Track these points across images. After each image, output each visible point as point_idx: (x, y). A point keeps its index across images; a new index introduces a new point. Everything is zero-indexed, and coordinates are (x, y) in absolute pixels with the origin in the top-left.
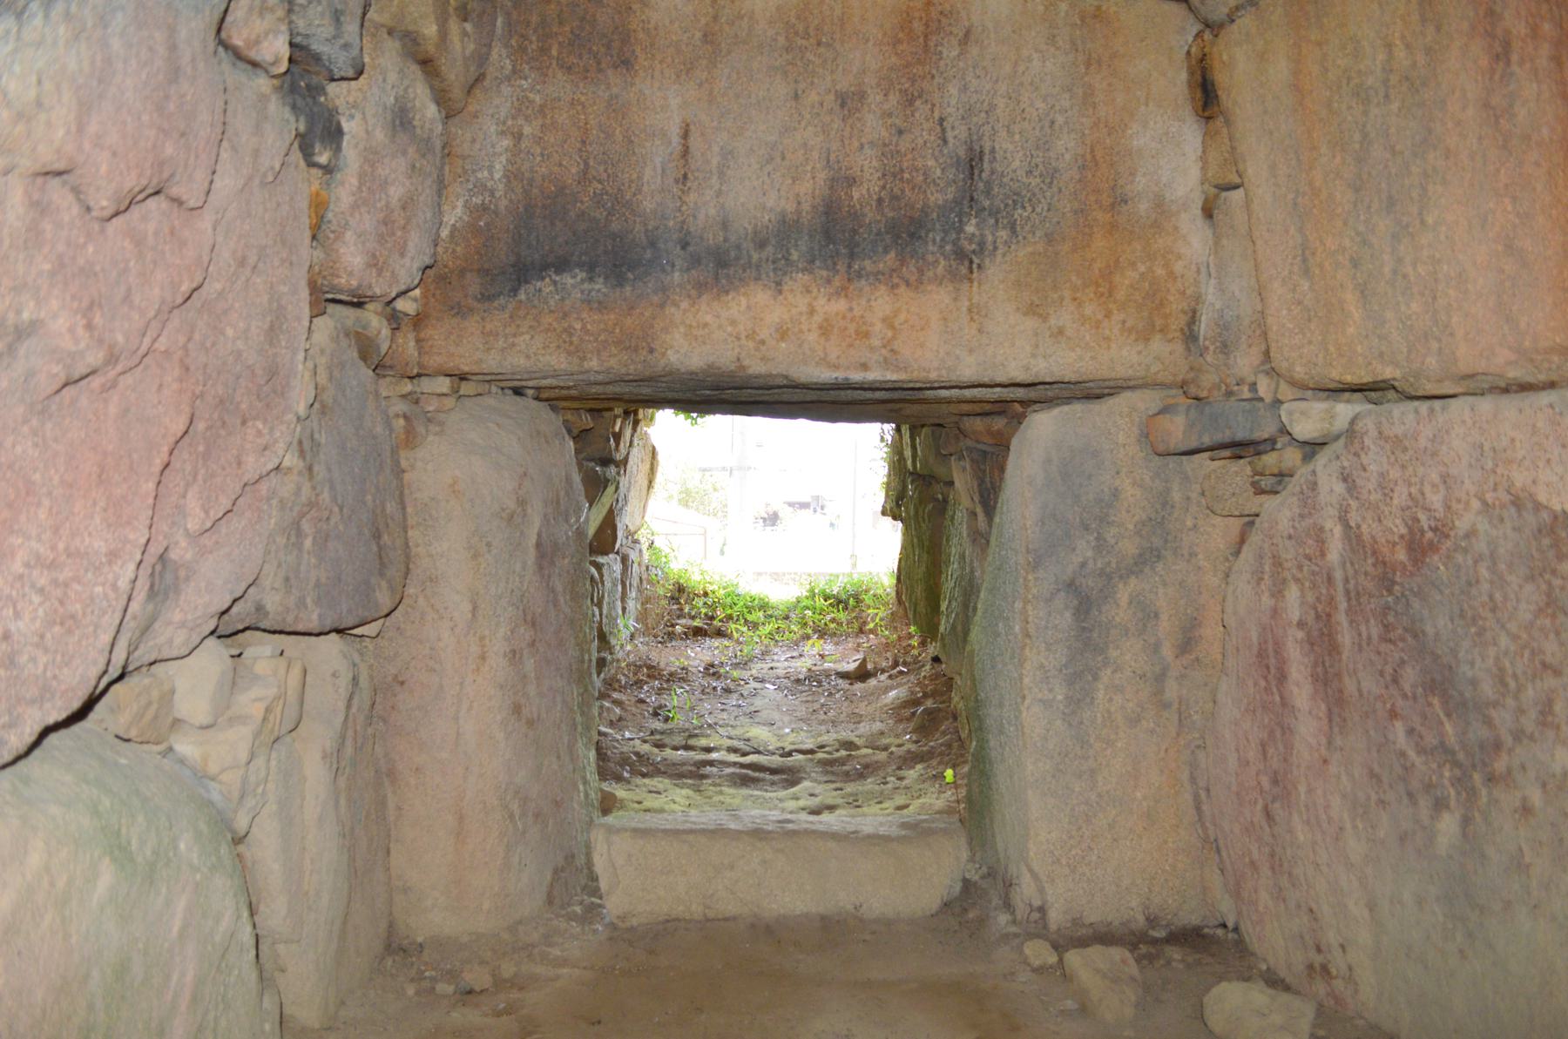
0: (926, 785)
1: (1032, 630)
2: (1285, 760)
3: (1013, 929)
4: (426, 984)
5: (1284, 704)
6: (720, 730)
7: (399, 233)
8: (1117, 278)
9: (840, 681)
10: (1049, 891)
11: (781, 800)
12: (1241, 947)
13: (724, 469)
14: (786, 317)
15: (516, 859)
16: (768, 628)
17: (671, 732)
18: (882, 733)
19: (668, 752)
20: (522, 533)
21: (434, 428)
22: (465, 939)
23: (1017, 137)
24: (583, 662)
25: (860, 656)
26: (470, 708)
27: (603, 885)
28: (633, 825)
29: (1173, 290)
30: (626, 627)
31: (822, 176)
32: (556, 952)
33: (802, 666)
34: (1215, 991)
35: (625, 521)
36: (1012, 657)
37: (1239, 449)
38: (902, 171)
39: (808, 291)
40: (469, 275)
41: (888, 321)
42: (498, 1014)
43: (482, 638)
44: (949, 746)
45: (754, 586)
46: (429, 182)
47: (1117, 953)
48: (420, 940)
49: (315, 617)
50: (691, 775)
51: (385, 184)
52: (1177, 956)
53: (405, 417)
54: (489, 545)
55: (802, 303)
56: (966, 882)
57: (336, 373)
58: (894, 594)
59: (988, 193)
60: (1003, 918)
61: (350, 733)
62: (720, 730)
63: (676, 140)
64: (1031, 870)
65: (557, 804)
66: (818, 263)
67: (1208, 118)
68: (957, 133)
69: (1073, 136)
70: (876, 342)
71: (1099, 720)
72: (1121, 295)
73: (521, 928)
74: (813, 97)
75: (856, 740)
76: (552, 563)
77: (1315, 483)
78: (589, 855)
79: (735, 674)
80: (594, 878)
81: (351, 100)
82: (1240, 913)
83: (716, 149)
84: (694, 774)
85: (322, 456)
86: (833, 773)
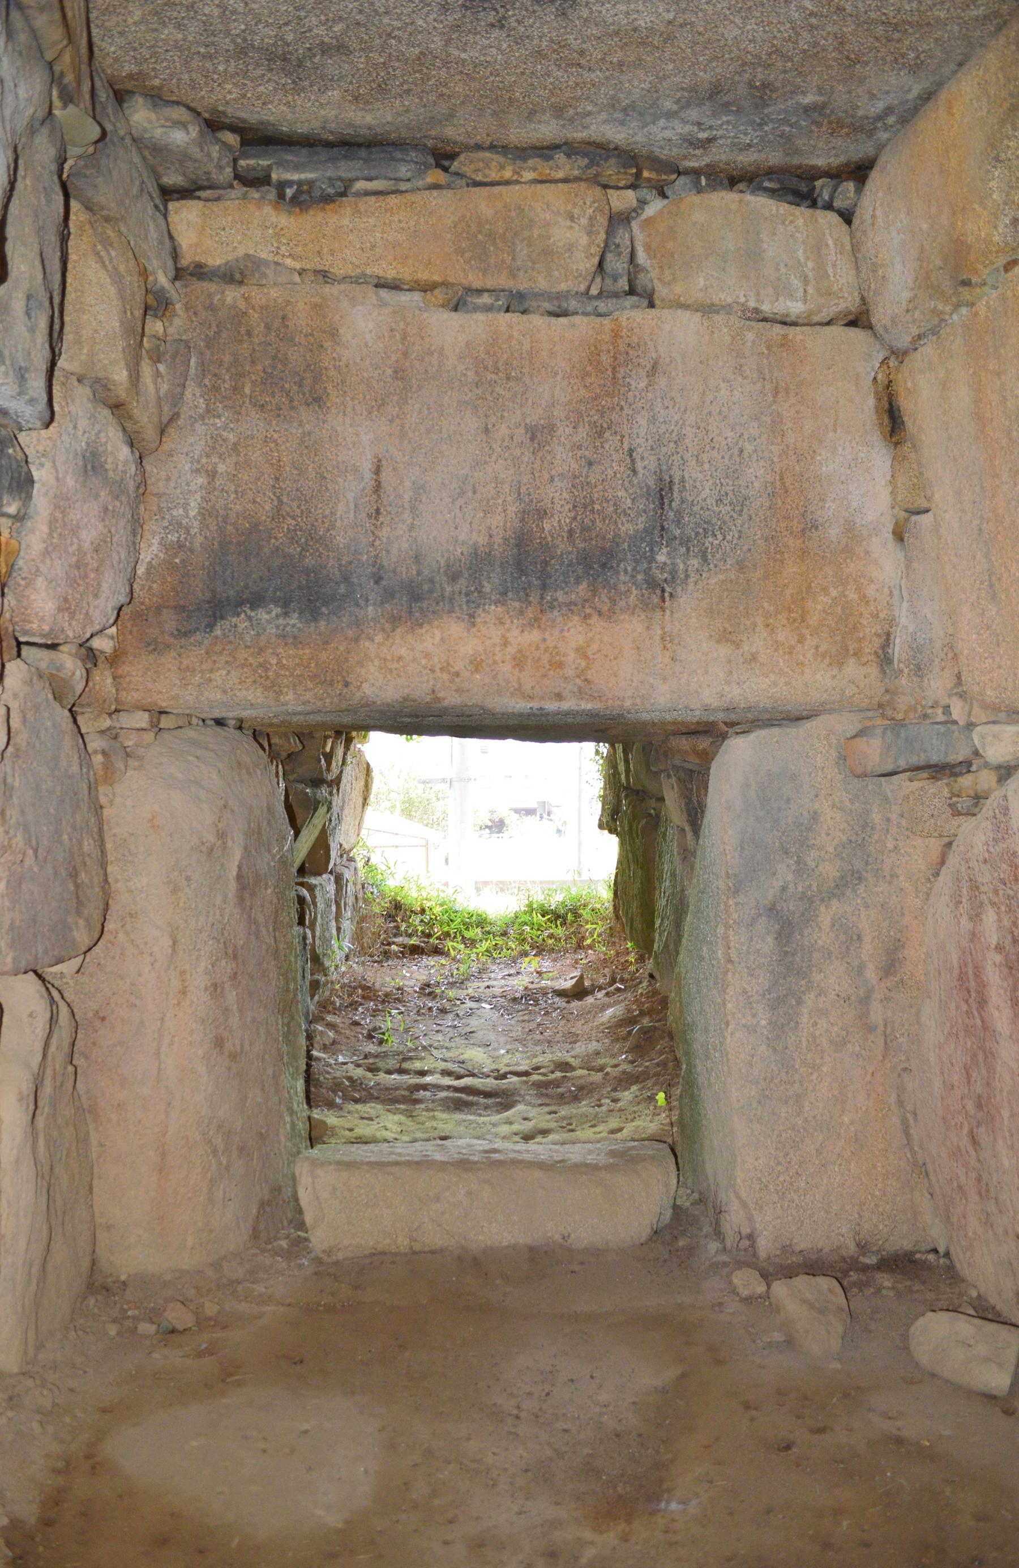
0: (640, 1107)
1: (734, 956)
2: (988, 1084)
3: (724, 1258)
4: (128, 1323)
5: (985, 1028)
6: (435, 1052)
7: (92, 576)
8: (809, 603)
9: (557, 999)
10: (758, 1219)
11: (494, 1125)
12: (952, 1274)
13: (444, 780)
14: (480, 649)
15: (220, 1194)
16: (485, 945)
17: (385, 1055)
18: (598, 1053)
19: (382, 1075)
20: (222, 865)
21: (132, 763)
22: (168, 1277)
23: (706, 466)
24: (288, 990)
25: (577, 973)
26: (171, 1044)
27: (308, 1218)
28: (338, 1157)
29: (865, 615)
30: (340, 948)
31: (513, 509)
32: (260, 1288)
33: (519, 984)
34: (921, 1321)
35: (340, 838)
36: (716, 983)
37: (938, 770)
38: (593, 502)
39: (502, 623)
40: (165, 611)
41: (582, 652)
42: (200, 1355)
43: (183, 973)
44: (664, 1064)
45: (474, 901)
46: (122, 523)
47: (825, 1283)
48: (123, 1278)
49: (9, 959)
50: (405, 1100)
51: (75, 530)
52: (888, 1284)
53: (104, 753)
54: (188, 879)
55: (495, 635)
56: (675, 1207)
57: (30, 716)
58: (611, 908)
59: (678, 522)
60: (713, 1246)
61: (49, 1072)
62: (435, 1052)
63: (368, 475)
64: (739, 1198)
65: (262, 1137)
66: (510, 595)
67: (897, 444)
68: (647, 464)
69: (762, 463)
70: (570, 672)
71: (804, 1044)
72: (813, 620)
73: (225, 1264)
74: (503, 430)
75: (571, 1060)
76: (253, 895)
77: (1007, 809)
78: (294, 1186)
79: (451, 994)
80: (300, 1211)
81: (41, 448)
82: (951, 1238)
83: (408, 483)
84: (406, 1099)
85: (15, 800)
86: (547, 1096)
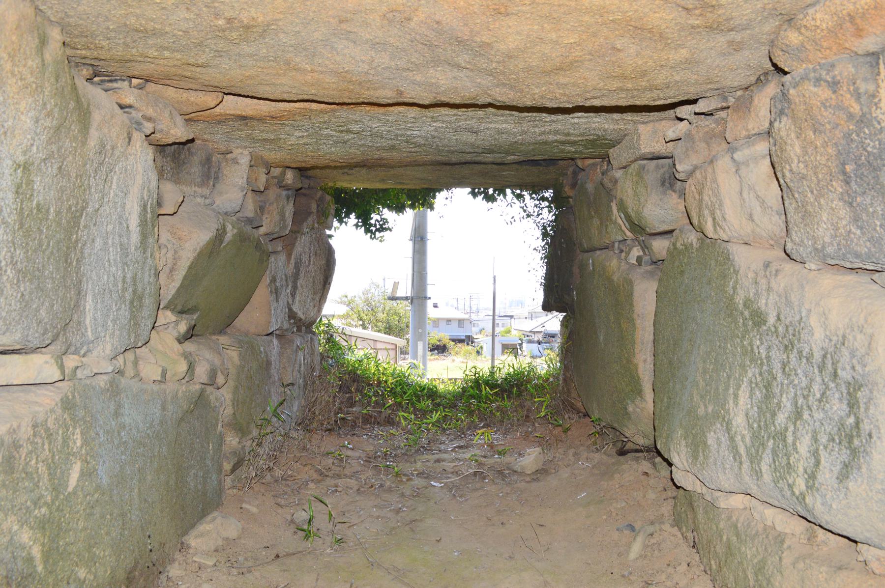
16: (436, 416)
